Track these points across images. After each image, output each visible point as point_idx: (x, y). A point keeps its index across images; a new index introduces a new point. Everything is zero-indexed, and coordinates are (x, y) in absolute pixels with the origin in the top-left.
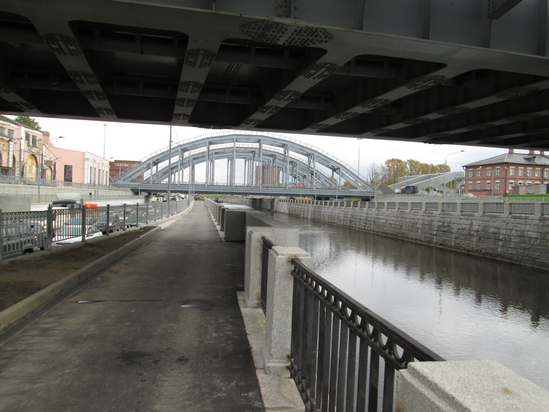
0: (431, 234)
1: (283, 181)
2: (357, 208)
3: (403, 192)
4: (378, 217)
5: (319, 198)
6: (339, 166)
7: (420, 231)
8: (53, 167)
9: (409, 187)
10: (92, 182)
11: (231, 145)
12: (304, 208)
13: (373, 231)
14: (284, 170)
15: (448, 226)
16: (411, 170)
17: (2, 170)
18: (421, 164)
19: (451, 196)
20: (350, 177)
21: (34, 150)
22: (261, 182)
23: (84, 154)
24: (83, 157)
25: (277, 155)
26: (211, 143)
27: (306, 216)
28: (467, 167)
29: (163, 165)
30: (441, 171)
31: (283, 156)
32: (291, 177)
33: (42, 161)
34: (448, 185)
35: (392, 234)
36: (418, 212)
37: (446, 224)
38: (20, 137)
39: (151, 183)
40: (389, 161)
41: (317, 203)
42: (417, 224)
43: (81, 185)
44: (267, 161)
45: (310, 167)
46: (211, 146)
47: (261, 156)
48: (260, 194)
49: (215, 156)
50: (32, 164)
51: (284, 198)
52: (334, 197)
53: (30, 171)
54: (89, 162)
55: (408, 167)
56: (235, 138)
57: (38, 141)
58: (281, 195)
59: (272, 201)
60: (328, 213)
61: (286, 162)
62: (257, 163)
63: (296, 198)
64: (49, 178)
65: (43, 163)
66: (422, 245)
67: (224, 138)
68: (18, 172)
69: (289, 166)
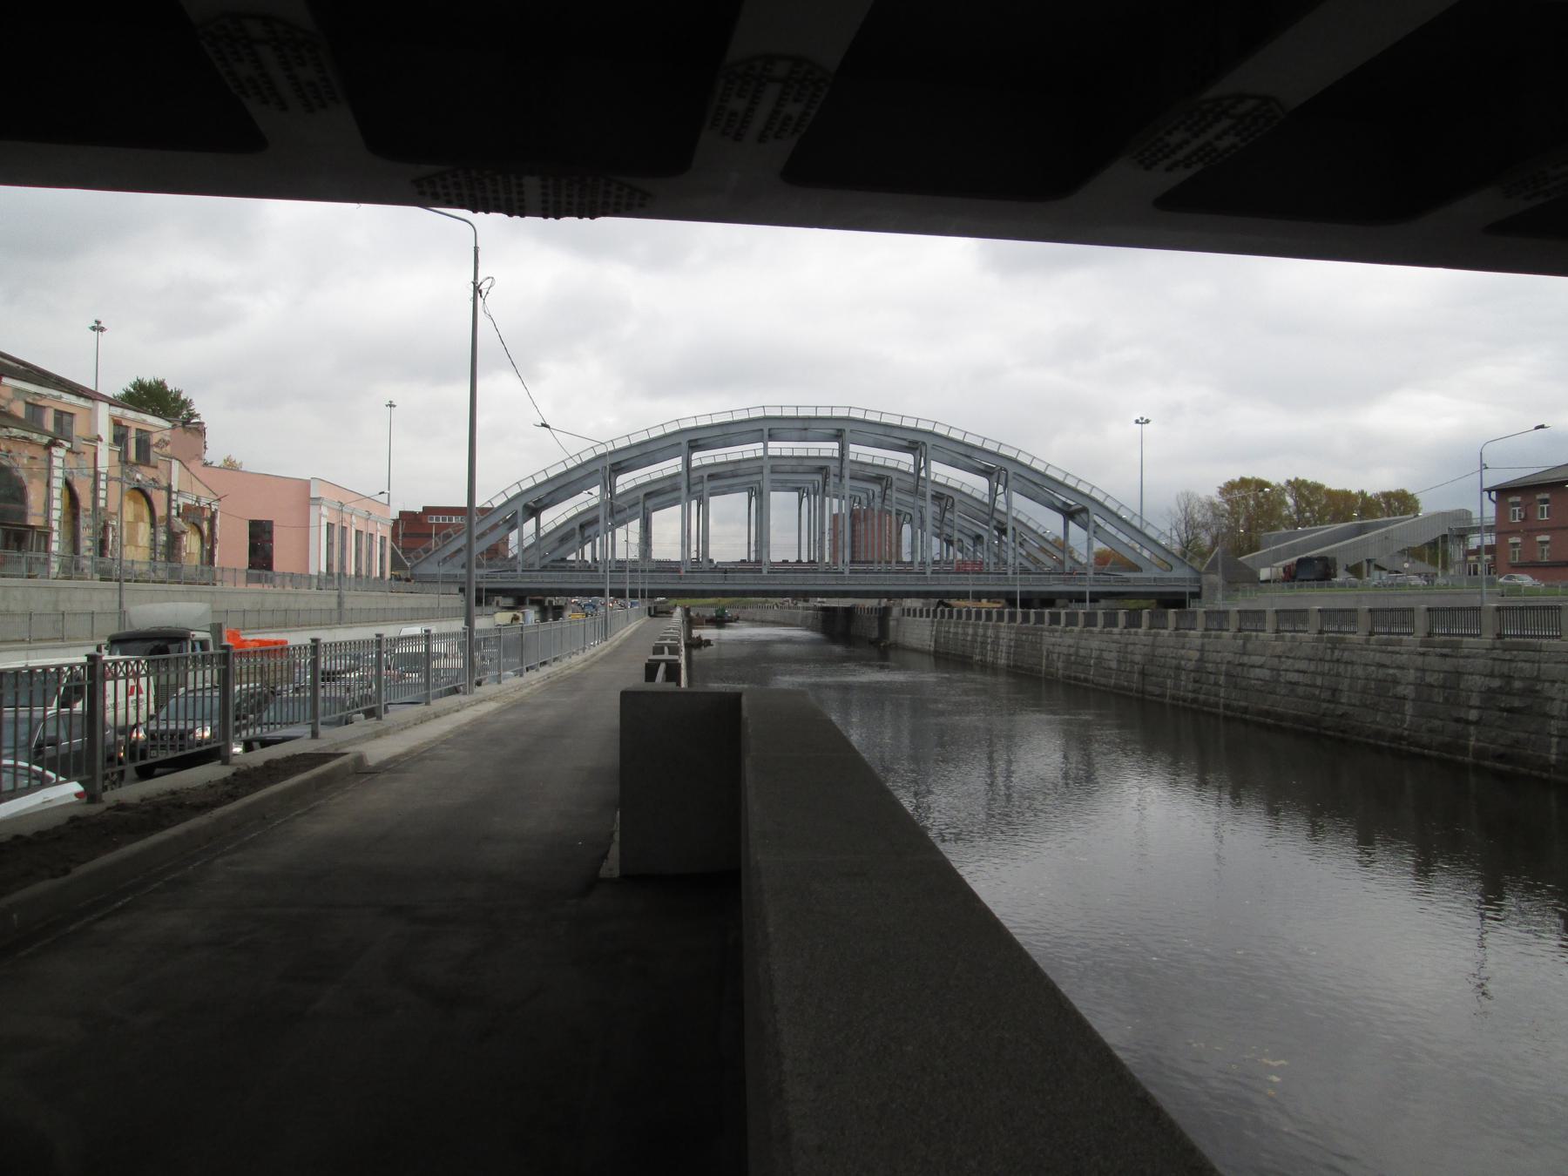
0: (1458, 720)
1: (913, 553)
2: (1116, 630)
3: (1293, 575)
4: (1245, 659)
5: (1028, 601)
6: (1087, 504)
7: (1409, 708)
8: (205, 526)
9: (1308, 561)
10: (336, 570)
11: (752, 450)
12: (985, 635)
13: (1227, 707)
14: (917, 522)
15: (1530, 692)
16: (1299, 511)
17: (7, 535)
18: (1330, 493)
19: (1452, 587)
20: (1121, 536)
21: (142, 475)
22: (847, 559)
23: (306, 485)
24: (303, 494)
25: (894, 476)
26: (695, 446)
27: (989, 659)
28: (1503, 492)
29: (552, 518)
30: (1390, 511)
31: (911, 480)
32: (936, 542)
33: (169, 508)
34: (1414, 553)
35: (1297, 719)
36: (1400, 643)
37: (1517, 684)
38: (92, 436)
39: (519, 569)
40: (1230, 487)
41: (1026, 618)
42: (1396, 682)
43: (300, 579)
44: (863, 496)
45: (994, 509)
46: (695, 455)
47: (847, 482)
48: (845, 594)
49: (708, 486)
50: (138, 518)
51: (916, 603)
52: (1079, 598)
53: (133, 540)
54: (324, 510)
55: (1290, 501)
56: (766, 427)
57: (157, 445)
58: (908, 595)
59: (884, 613)
60: (1065, 650)
61: (924, 495)
62: (835, 501)
63: (953, 602)
64: (196, 560)
65: (174, 512)
66: (1424, 757)
67: (733, 429)
68: (88, 543)
69: (931, 509)
